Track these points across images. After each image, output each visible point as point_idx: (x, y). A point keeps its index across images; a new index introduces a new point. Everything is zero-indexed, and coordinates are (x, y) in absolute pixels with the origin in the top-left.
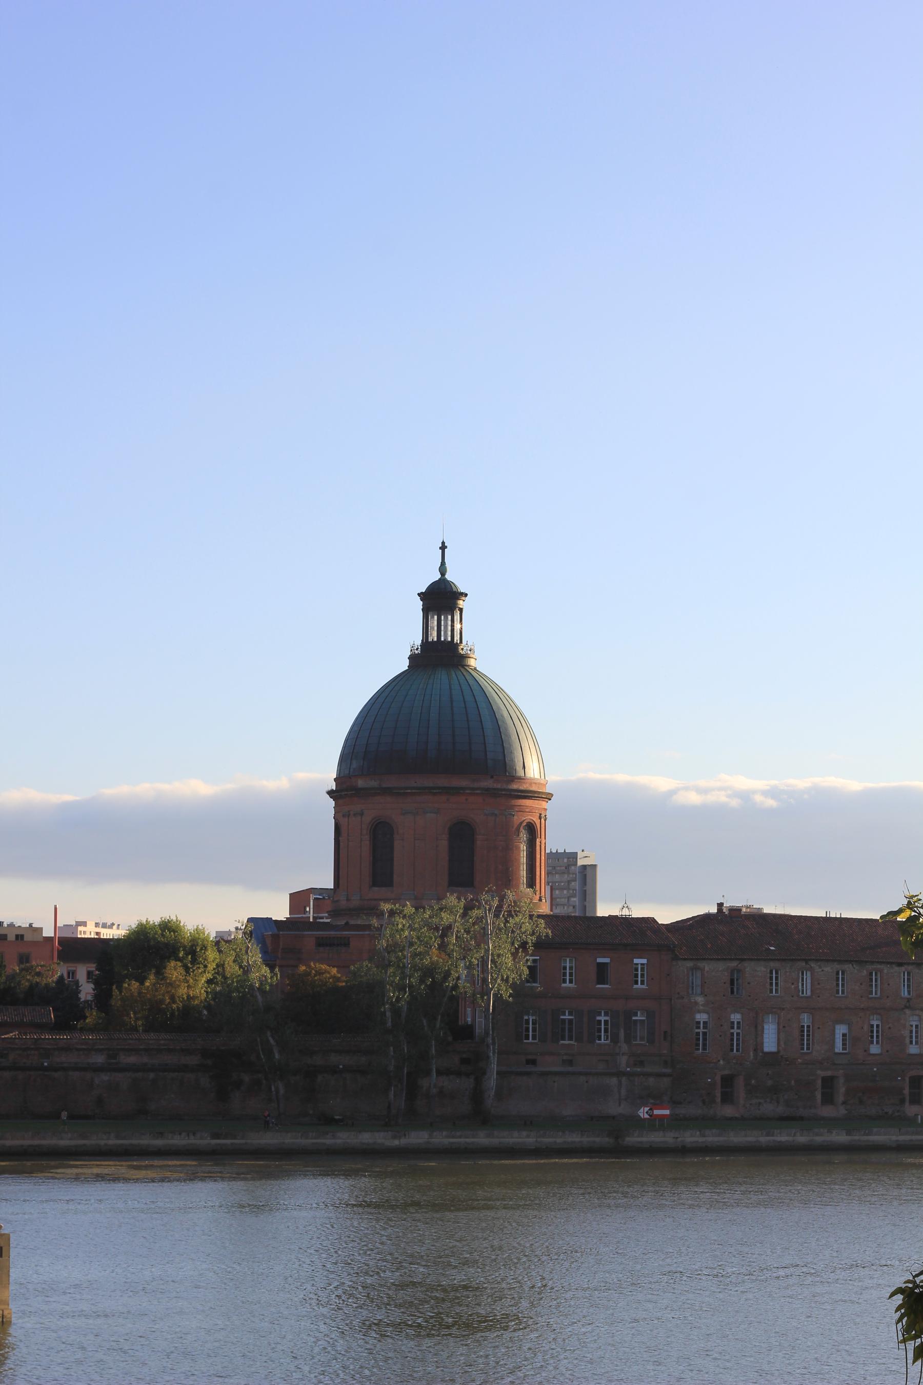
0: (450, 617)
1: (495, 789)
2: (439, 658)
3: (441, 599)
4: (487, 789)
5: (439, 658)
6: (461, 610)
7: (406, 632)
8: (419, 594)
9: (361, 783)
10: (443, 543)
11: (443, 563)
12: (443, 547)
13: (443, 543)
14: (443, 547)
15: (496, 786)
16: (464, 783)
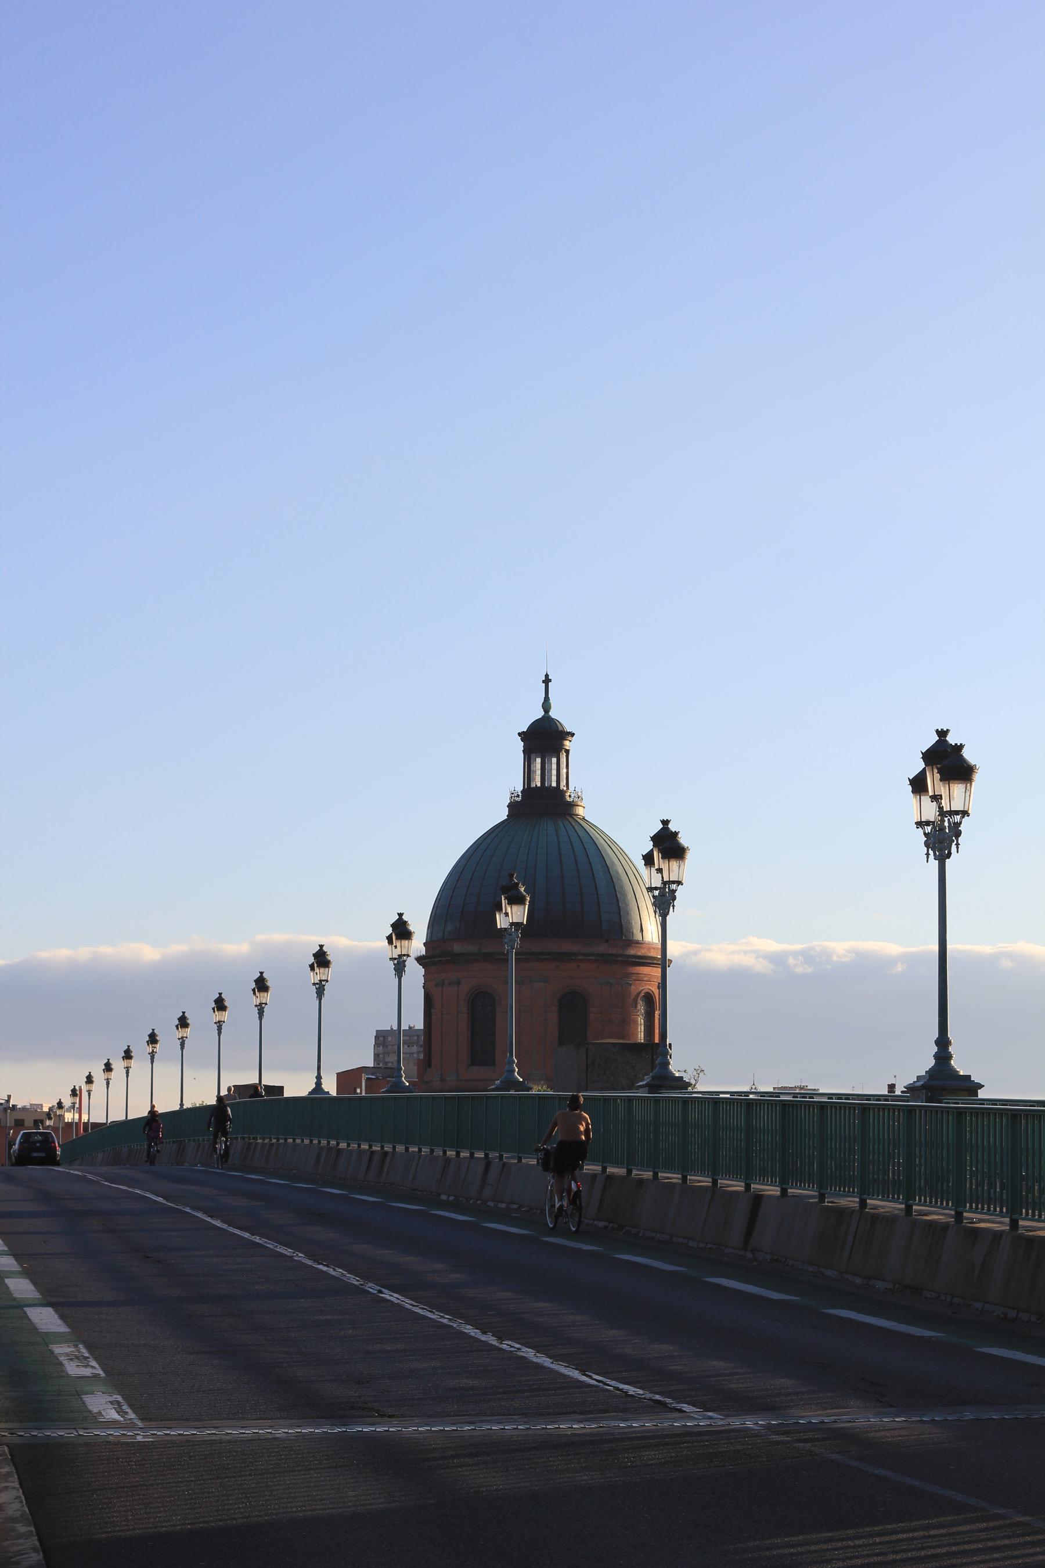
0: (554, 760)
1: (610, 955)
2: (543, 807)
3: (545, 739)
4: (602, 955)
5: (543, 807)
6: (567, 752)
7: (505, 777)
8: (519, 734)
9: (457, 948)
10: (547, 676)
11: (547, 698)
12: (547, 681)
13: (547, 676)
14: (547, 681)
15: (611, 951)
16: (576, 948)
